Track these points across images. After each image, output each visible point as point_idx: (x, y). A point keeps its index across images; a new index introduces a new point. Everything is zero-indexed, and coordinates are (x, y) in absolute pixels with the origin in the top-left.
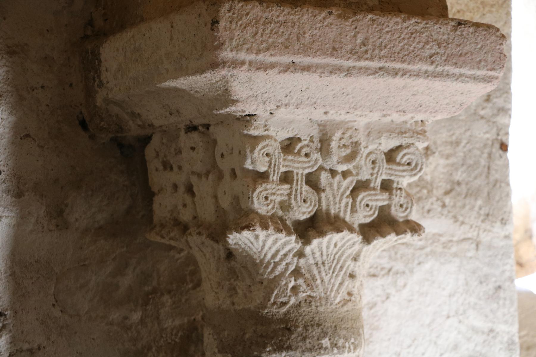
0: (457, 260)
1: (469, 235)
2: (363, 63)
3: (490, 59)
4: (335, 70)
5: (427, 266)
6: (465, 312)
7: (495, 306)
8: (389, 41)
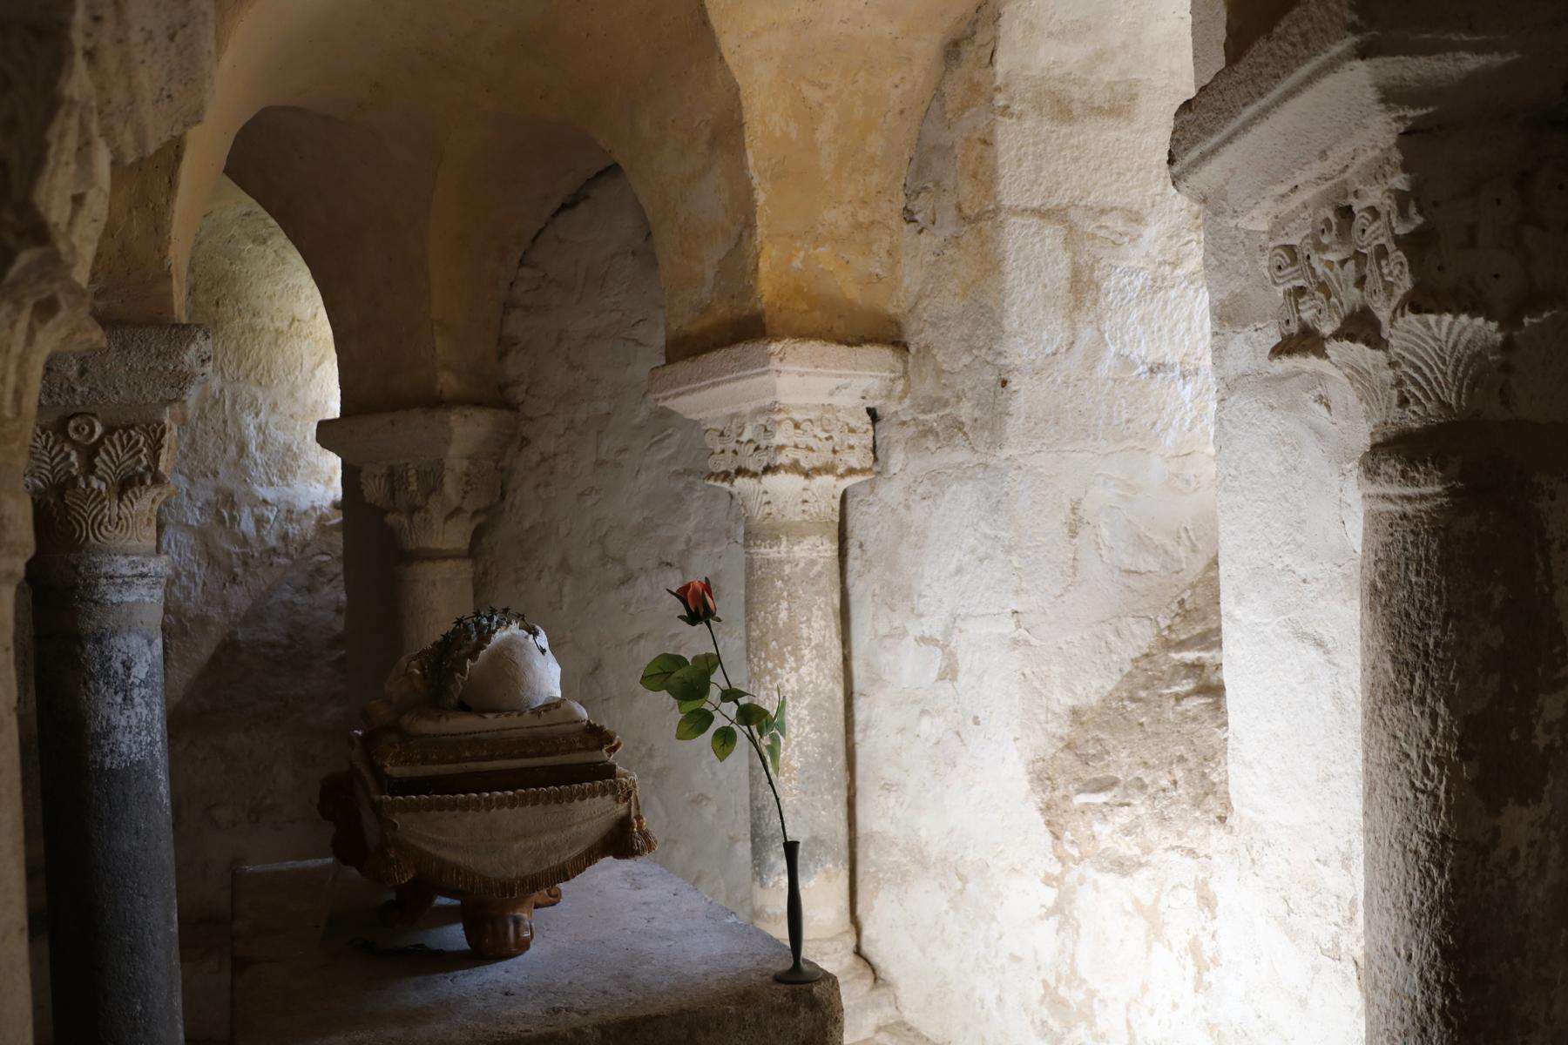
0: (970, 482)
1: (981, 461)
2: (703, 383)
3: (761, 360)
4: (693, 390)
5: (954, 488)
6: (978, 523)
7: (996, 516)
8: (1170, 238)
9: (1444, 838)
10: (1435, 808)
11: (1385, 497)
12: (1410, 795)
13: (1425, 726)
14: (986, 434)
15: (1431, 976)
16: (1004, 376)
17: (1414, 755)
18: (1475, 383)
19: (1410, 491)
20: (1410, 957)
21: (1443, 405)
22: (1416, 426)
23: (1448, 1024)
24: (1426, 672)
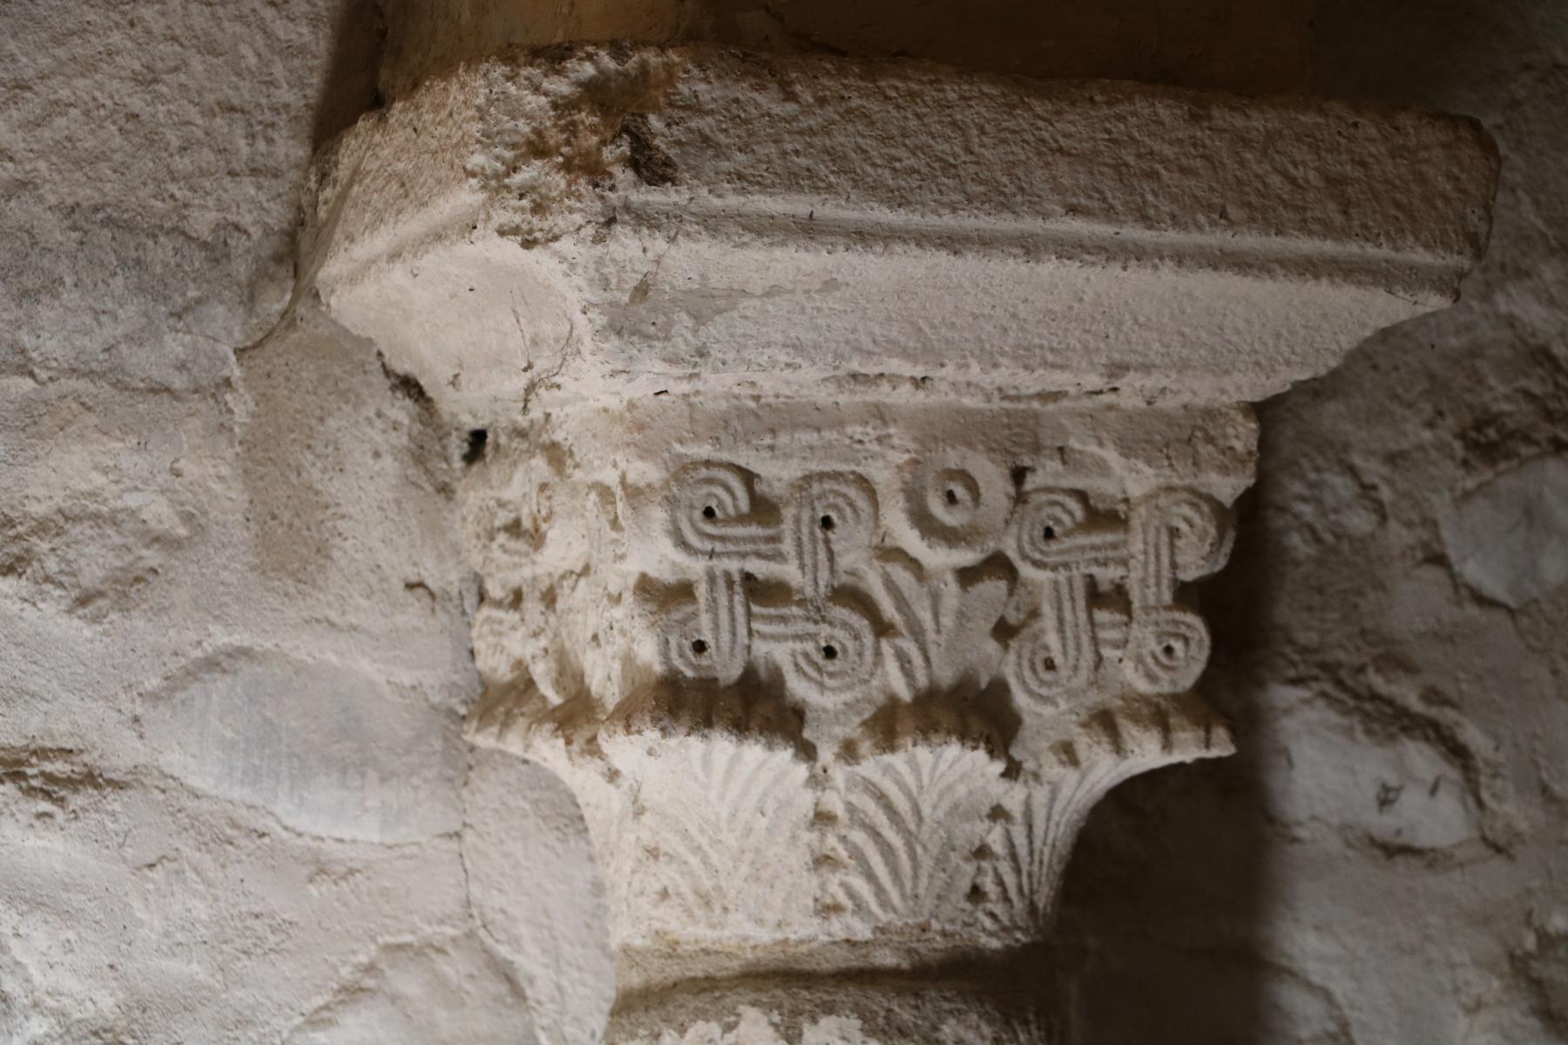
22: (995, 944)
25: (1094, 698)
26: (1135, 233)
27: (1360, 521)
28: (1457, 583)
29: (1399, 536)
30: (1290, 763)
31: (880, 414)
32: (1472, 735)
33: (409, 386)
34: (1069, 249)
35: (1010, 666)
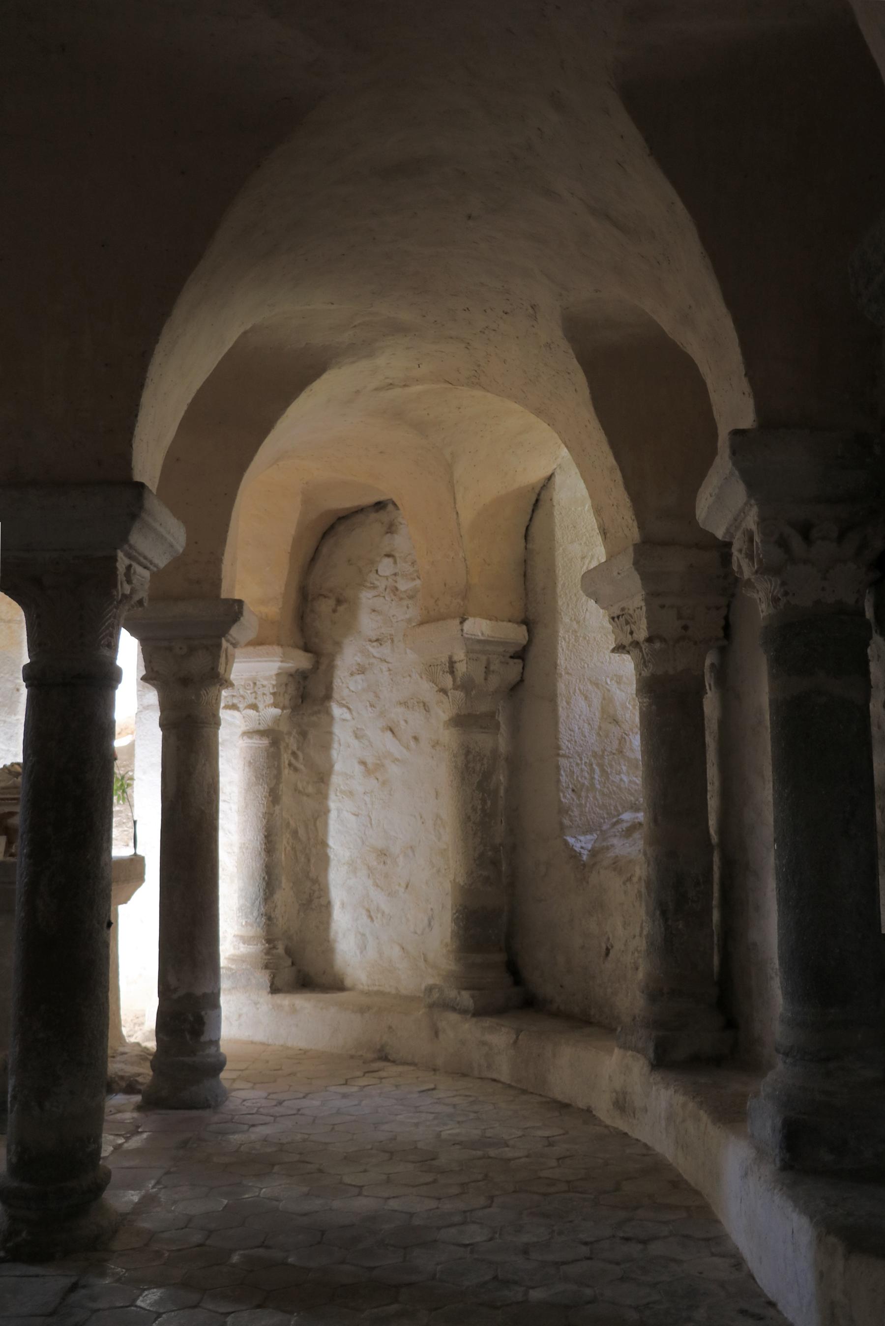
9: (266, 813)
10: (264, 807)
11: (254, 743)
12: (258, 805)
13: (263, 790)
14: (6, 708)
15: (262, 842)
16: (17, 687)
17: (260, 796)
18: (274, 722)
19: (261, 742)
20: (257, 839)
21: (268, 725)
23: (265, 851)
24: (263, 779)
25: (265, 704)
26: (249, 660)
27: (341, 684)
28: (350, 690)
29: (344, 685)
30: (718, 720)
31: (241, 679)
32: (351, 707)
33: (457, 513)
34: (244, 662)
35: (257, 702)
